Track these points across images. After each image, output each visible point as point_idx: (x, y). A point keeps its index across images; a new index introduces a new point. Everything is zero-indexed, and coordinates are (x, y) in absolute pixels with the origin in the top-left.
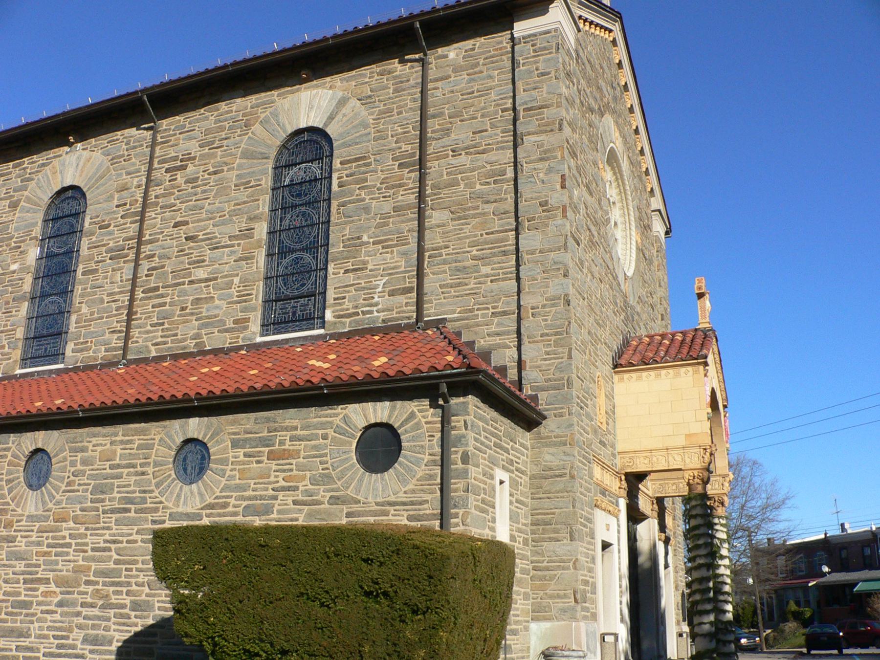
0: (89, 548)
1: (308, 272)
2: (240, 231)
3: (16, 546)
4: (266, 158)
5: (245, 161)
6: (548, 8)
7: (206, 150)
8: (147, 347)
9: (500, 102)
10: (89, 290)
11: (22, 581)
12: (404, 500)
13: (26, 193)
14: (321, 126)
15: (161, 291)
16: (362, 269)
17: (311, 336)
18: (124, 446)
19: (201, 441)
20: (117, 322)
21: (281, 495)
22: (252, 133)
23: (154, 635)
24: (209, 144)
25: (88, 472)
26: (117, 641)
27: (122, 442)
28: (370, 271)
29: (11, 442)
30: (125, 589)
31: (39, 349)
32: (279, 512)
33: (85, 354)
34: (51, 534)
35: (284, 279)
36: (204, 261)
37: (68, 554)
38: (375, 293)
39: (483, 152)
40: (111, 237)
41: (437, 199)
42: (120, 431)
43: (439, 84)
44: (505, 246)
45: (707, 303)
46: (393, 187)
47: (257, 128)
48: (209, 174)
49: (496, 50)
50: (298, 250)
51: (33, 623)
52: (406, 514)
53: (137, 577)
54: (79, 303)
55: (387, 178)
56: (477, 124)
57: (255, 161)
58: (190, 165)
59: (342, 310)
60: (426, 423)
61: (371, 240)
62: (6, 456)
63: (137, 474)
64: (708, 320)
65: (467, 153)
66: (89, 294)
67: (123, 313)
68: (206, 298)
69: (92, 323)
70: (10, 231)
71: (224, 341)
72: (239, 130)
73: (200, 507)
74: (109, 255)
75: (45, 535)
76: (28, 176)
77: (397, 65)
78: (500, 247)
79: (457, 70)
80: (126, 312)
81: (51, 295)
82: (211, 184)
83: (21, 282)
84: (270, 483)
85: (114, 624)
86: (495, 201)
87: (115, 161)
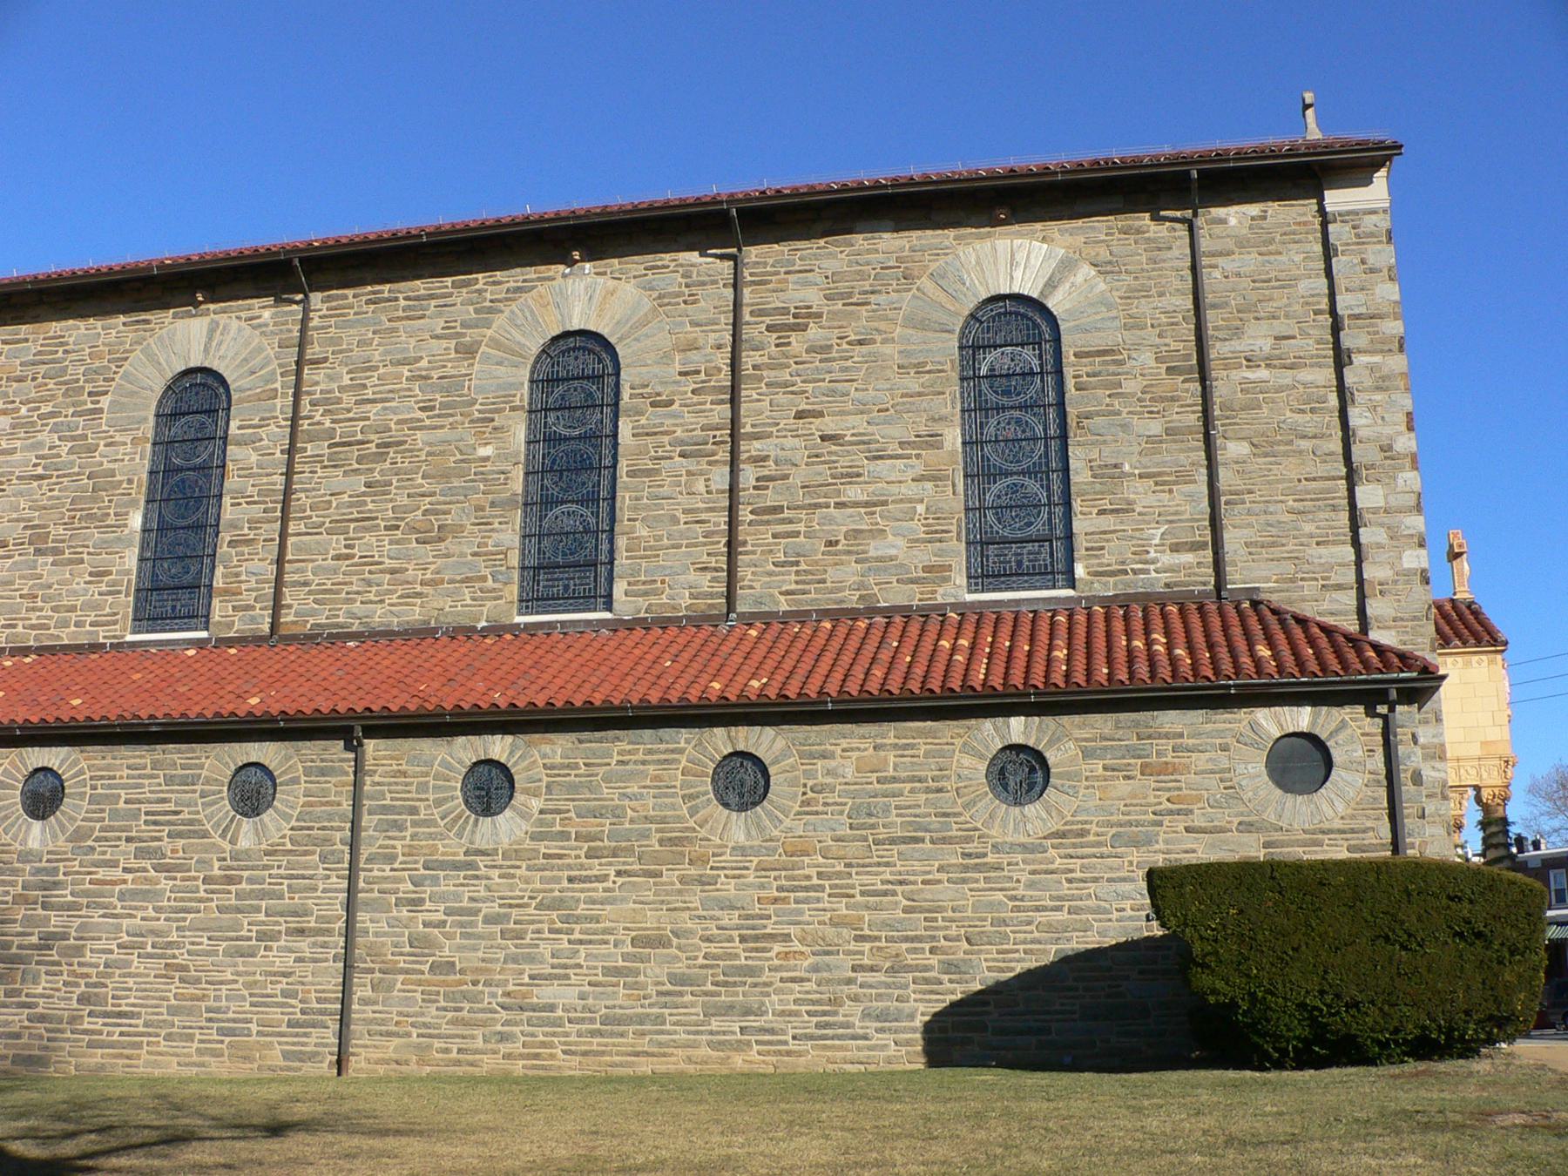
0: (856, 892)
1: (1035, 506)
2: (917, 436)
3: (718, 890)
4: (949, 331)
5: (911, 331)
6: (1372, 177)
7: (839, 305)
8: (772, 595)
9: (1311, 299)
10: (645, 501)
11: (737, 939)
12: (1342, 827)
13: (489, 332)
14: (1035, 296)
15: (787, 514)
16: (1127, 511)
17: (1055, 598)
18: (900, 752)
19: (1033, 749)
20: (708, 554)
21: (1167, 820)
22: (918, 289)
23: (986, 1003)
24: (842, 296)
25: (838, 787)
26: (923, 1014)
27: (895, 746)
28: (1139, 514)
29: (683, 741)
30: (927, 946)
31: (553, 586)
32: (1166, 842)
33: (653, 600)
34: (783, 873)
35: (997, 513)
36: (859, 475)
37: (818, 900)
38: (1150, 545)
39: (1291, 367)
40: (677, 422)
41: (1230, 424)
42: (889, 732)
43: (1220, 261)
44: (1334, 498)
45: (1464, 565)
46: (1162, 399)
47: (925, 282)
48: (849, 343)
49: (1299, 224)
50: (1015, 473)
51: (769, 996)
52: (1346, 844)
53: (946, 928)
54: (629, 520)
55: (1152, 385)
56: (1282, 327)
57: (930, 334)
58: (811, 325)
59: (1100, 565)
60: (1363, 735)
61: (1137, 472)
62: (678, 761)
63: (928, 790)
64: (1466, 589)
65: (1268, 366)
66: (647, 508)
67: (719, 542)
68: (871, 530)
69: (661, 552)
70: (466, 391)
71: (911, 596)
72: (894, 283)
73: (1041, 835)
74: (678, 449)
75: (773, 874)
76: (488, 304)
77: (1148, 222)
78: (1326, 499)
79: (1242, 244)
80: (724, 540)
81: (563, 502)
82: (856, 359)
83: (502, 476)
84: (1150, 805)
85: (914, 992)
86: (1315, 437)
87: (666, 301)
